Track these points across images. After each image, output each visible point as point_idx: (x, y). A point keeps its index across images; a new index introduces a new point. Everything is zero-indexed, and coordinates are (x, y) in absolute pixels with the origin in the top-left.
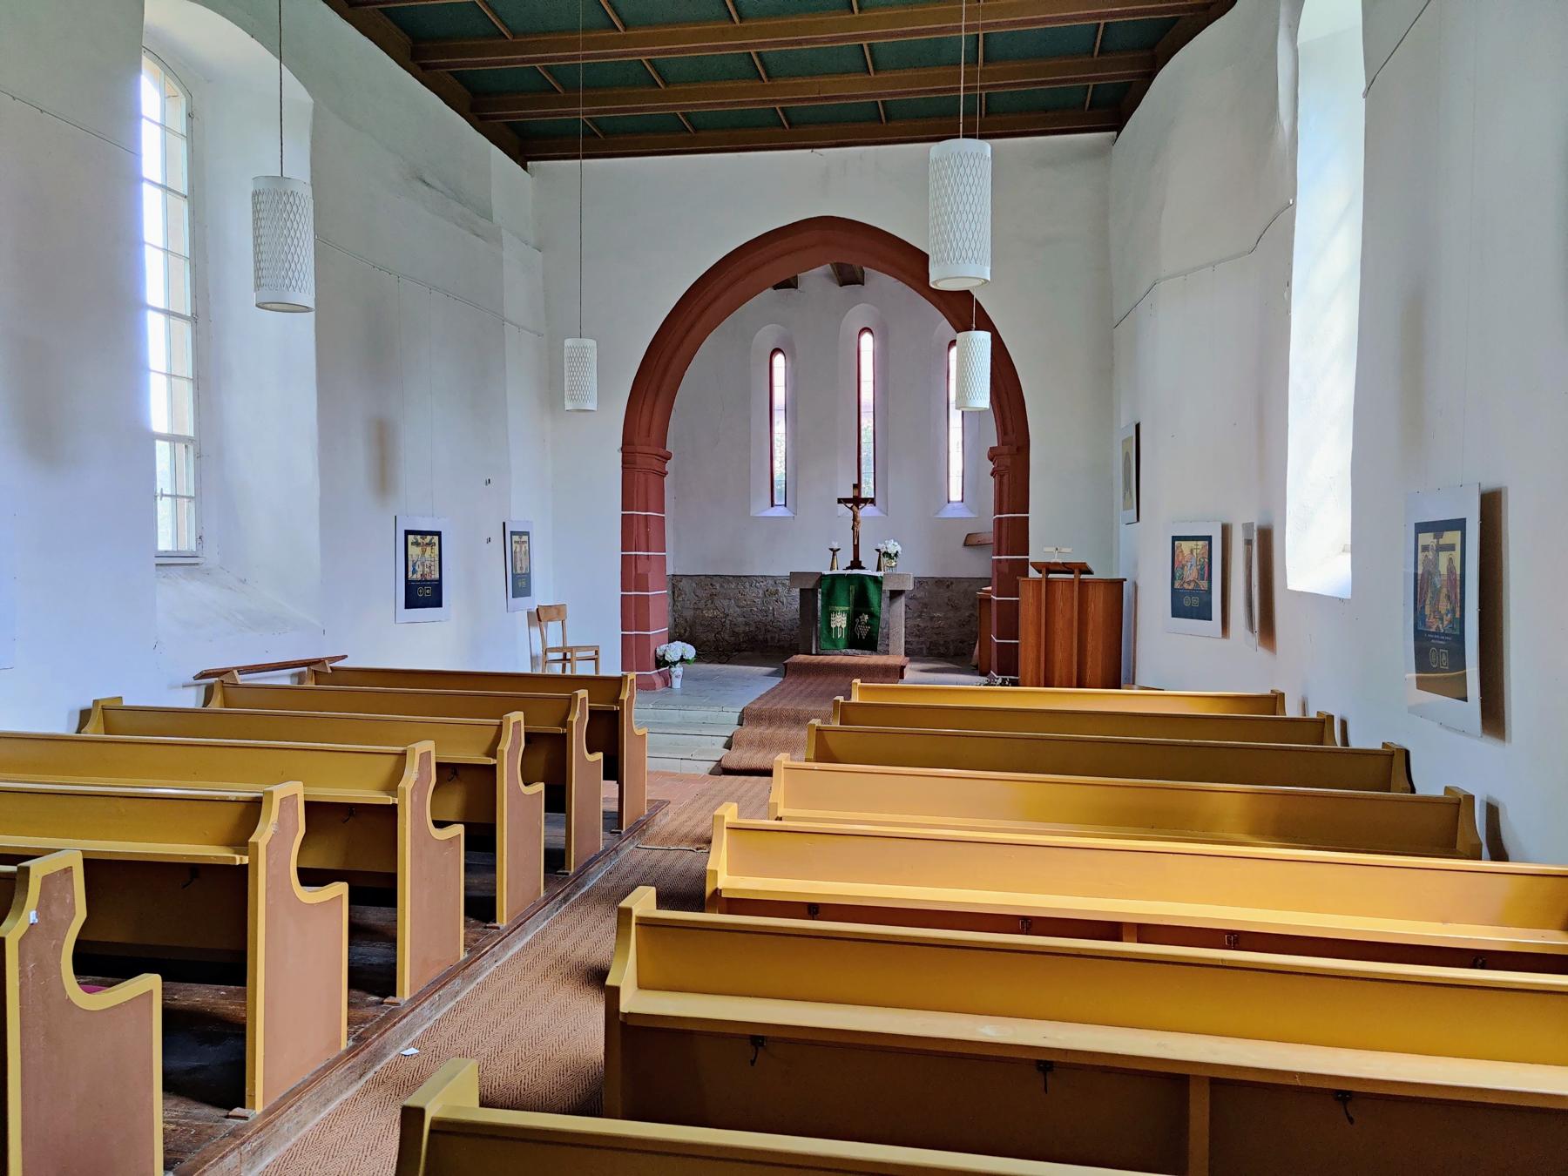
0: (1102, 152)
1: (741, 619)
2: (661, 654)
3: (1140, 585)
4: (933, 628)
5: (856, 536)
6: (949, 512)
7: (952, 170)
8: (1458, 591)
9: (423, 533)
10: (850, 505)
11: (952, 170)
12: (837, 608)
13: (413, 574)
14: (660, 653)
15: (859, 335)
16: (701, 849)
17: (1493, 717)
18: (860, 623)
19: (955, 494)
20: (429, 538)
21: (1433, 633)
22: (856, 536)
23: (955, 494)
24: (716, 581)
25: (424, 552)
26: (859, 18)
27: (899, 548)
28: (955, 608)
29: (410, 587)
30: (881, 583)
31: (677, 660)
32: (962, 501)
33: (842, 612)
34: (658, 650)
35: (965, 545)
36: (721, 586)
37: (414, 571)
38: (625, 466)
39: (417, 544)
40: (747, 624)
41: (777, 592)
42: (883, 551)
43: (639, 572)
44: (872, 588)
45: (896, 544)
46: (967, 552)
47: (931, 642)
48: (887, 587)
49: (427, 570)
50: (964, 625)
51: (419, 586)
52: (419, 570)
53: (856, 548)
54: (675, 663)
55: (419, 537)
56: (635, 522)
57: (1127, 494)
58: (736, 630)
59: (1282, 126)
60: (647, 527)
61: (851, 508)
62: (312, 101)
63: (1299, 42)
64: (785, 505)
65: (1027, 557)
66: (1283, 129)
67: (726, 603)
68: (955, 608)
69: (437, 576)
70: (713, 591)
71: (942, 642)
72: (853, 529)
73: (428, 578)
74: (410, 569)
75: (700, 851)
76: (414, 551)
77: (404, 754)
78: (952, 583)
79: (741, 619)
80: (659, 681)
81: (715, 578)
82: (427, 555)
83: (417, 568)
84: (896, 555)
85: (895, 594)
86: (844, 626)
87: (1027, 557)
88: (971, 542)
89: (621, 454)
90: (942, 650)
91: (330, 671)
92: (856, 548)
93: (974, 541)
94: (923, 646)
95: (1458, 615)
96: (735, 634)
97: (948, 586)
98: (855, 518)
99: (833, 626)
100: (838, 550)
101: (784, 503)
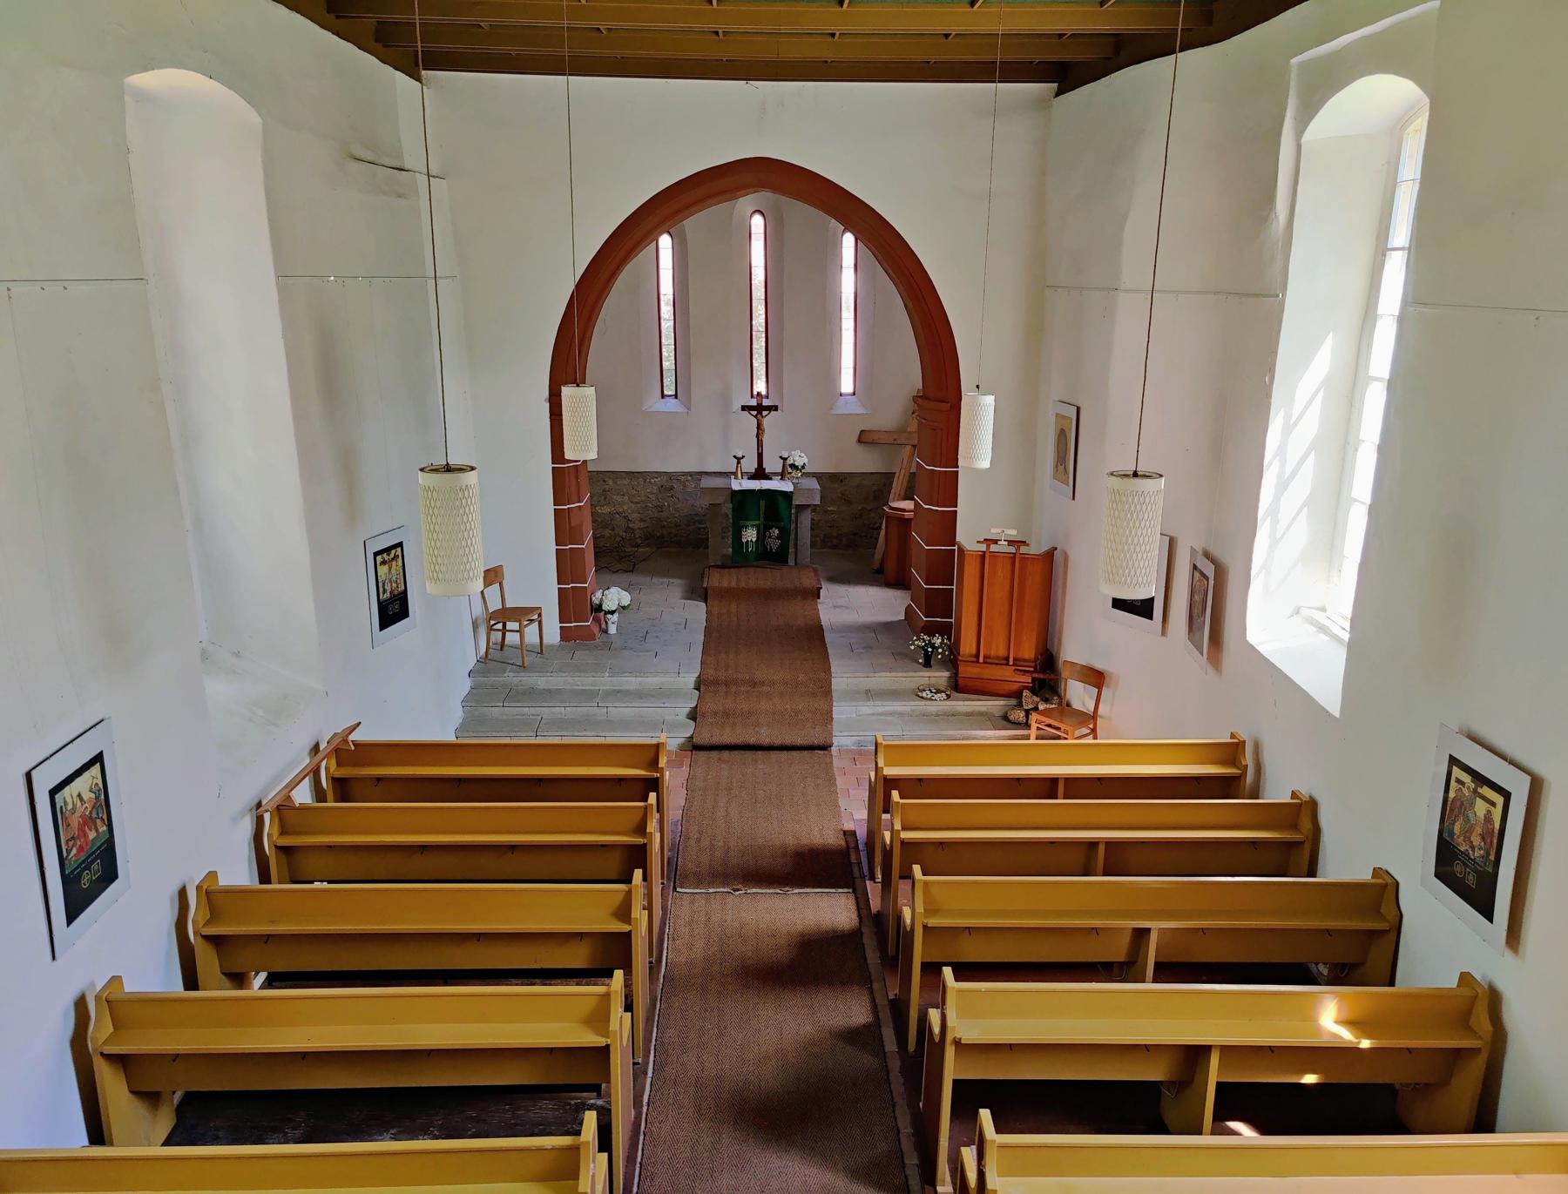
0: (1042, 104)
1: (635, 515)
2: (597, 603)
3: (1071, 557)
4: (826, 522)
5: (760, 444)
6: (842, 408)
7: (1136, 506)
8: (1495, 841)
9: (388, 550)
10: (754, 413)
11: (1136, 506)
12: (748, 523)
13: (384, 594)
14: (596, 601)
15: (751, 216)
16: (738, 890)
17: (1514, 936)
18: (770, 537)
19: (847, 385)
20: (393, 551)
21: (1462, 852)
22: (760, 444)
23: (847, 385)
24: (610, 478)
25: (390, 568)
26: (847, 11)
27: (805, 460)
28: (849, 502)
29: (383, 607)
30: (791, 498)
31: (614, 609)
32: (854, 394)
33: (753, 526)
34: (593, 599)
35: (860, 441)
36: (615, 482)
37: (385, 591)
38: (553, 417)
39: (384, 562)
40: (642, 520)
41: (672, 488)
42: (790, 461)
43: (572, 525)
44: (782, 503)
45: (803, 455)
46: (859, 449)
47: (825, 535)
48: (796, 502)
49: (394, 585)
50: (856, 518)
51: (388, 605)
52: (388, 588)
53: (760, 456)
54: (612, 613)
55: (385, 555)
56: (566, 472)
57: (1061, 468)
58: (631, 525)
59: (1277, 217)
60: (577, 478)
61: (755, 417)
62: (259, 120)
63: (1303, 140)
64: (676, 396)
65: (955, 509)
66: (1278, 221)
67: (619, 498)
68: (849, 502)
69: (403, 588)
70: (606, 486)
71: (835, 534)
72: (757, 436)
73: (396, 593)
74: (381, 590)
75: (737, 893)
76: (383, 570)
77: (607, 995)
78: (846, 478)
79: (635, 515)
80: (596, 630)
81: (608, 474)
82: (393, 571)
83: (386, 587)
84: (803, 467)
85: (801, 508)
86: (754, 540)
87: (955, 509)
88: (864, 438)
89: (548, 404)
90: (835, 542)
91: (353, 748)
92: (760, 456)
93: (869, 438)
94: (818, 539)
95: (1492, 857)
96: (627, 530)
97: (842, 481)
98: (759, 426)
99: (744, 540)
100: (743, 457)
101: (674, 393)
